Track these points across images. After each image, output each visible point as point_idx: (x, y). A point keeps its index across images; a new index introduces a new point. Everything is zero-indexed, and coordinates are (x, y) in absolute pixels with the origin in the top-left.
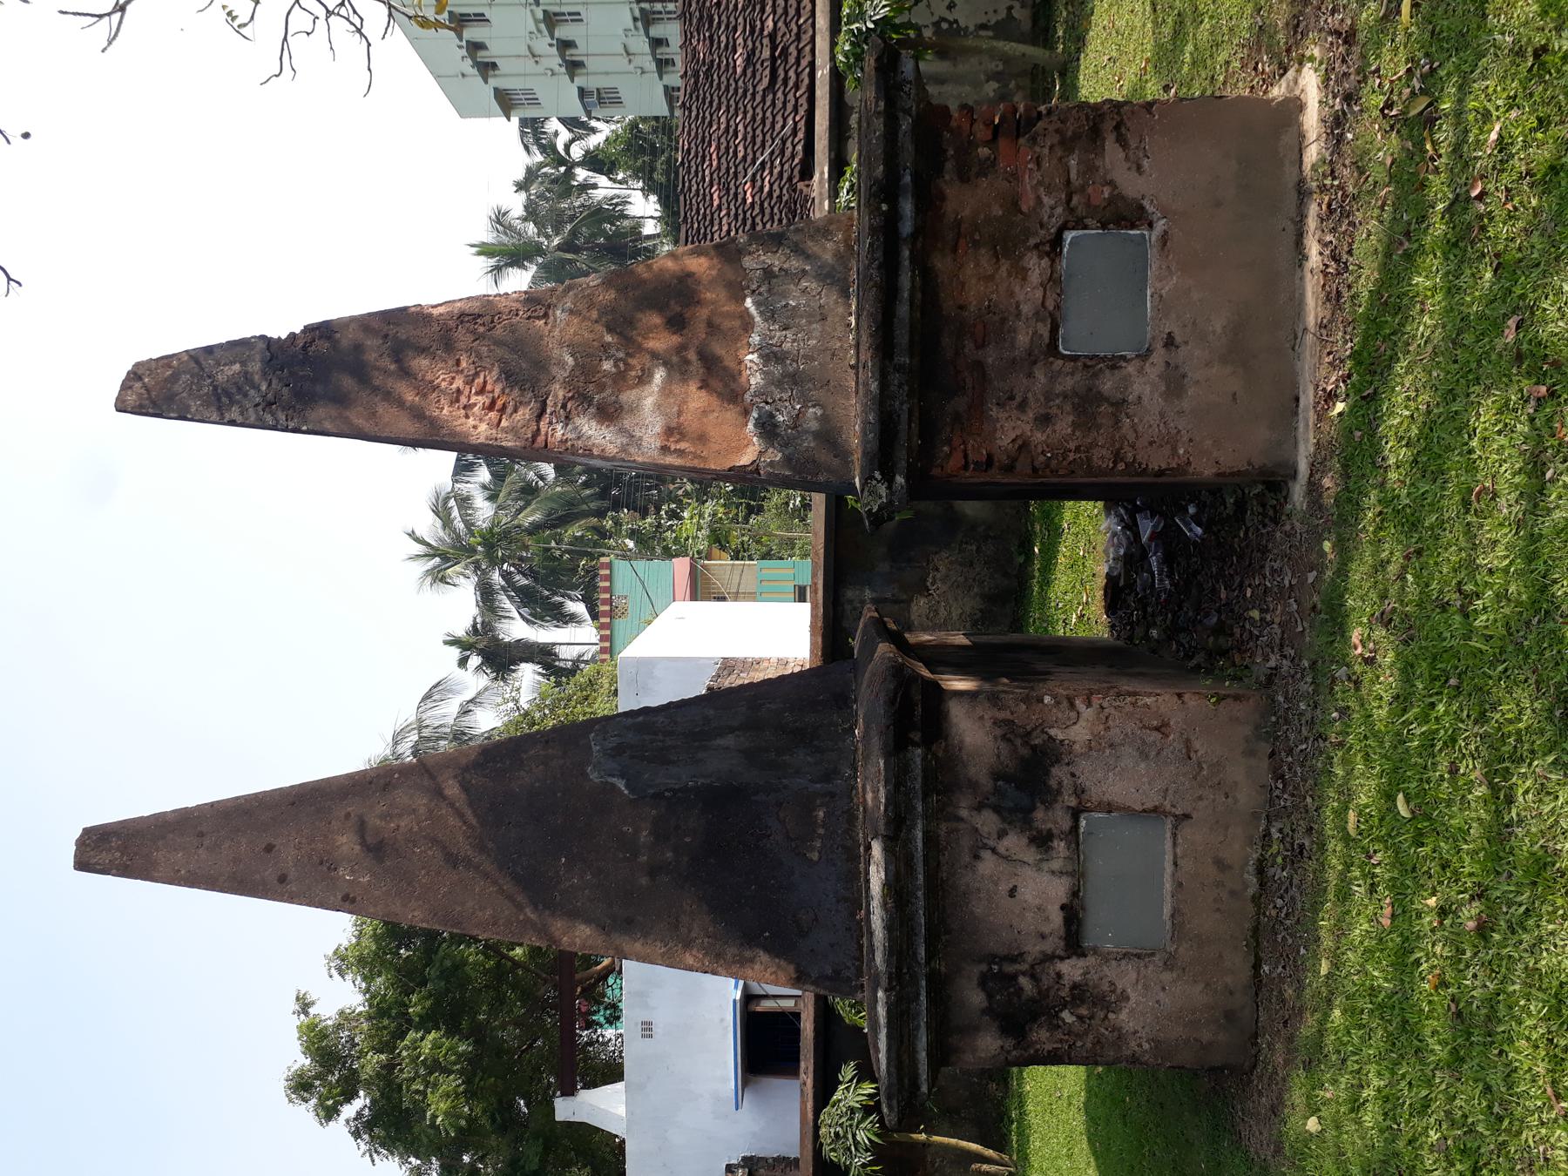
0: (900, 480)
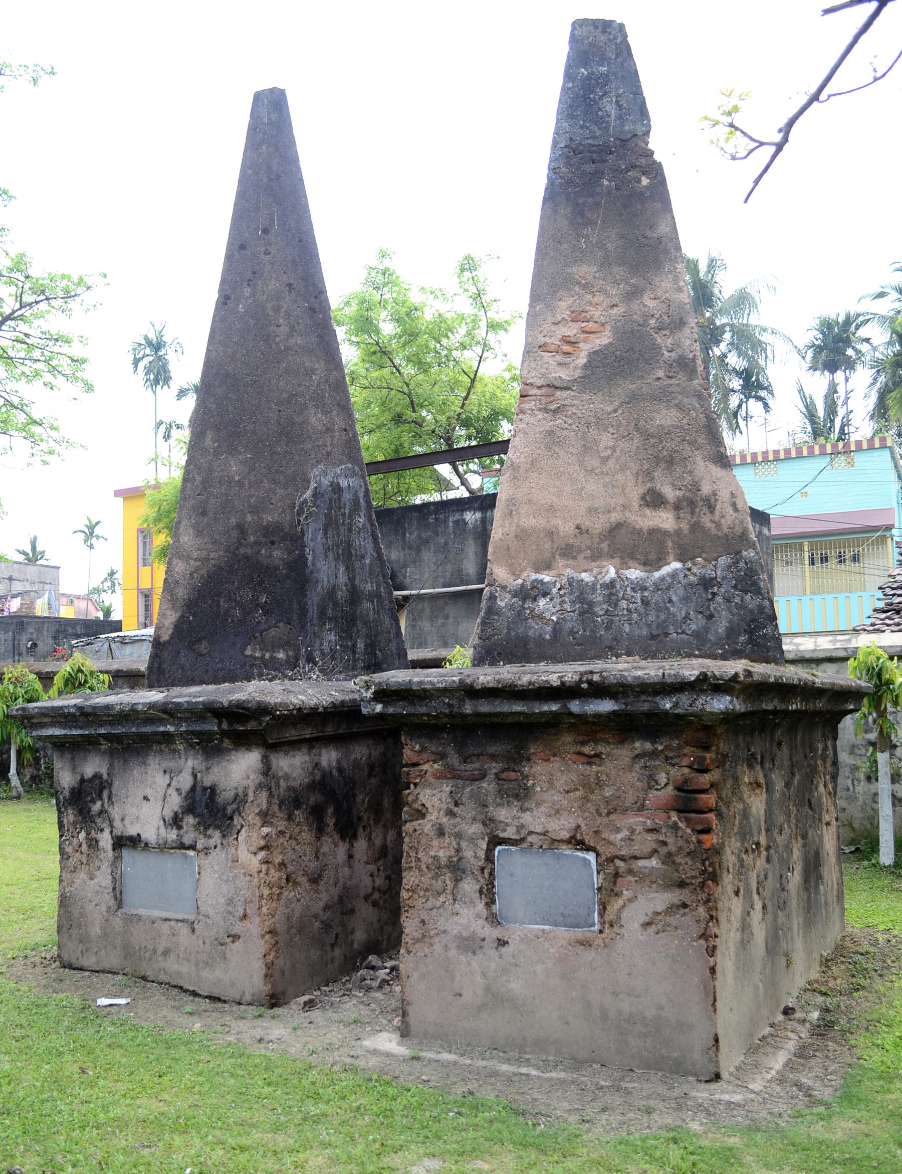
0: (379, 708)
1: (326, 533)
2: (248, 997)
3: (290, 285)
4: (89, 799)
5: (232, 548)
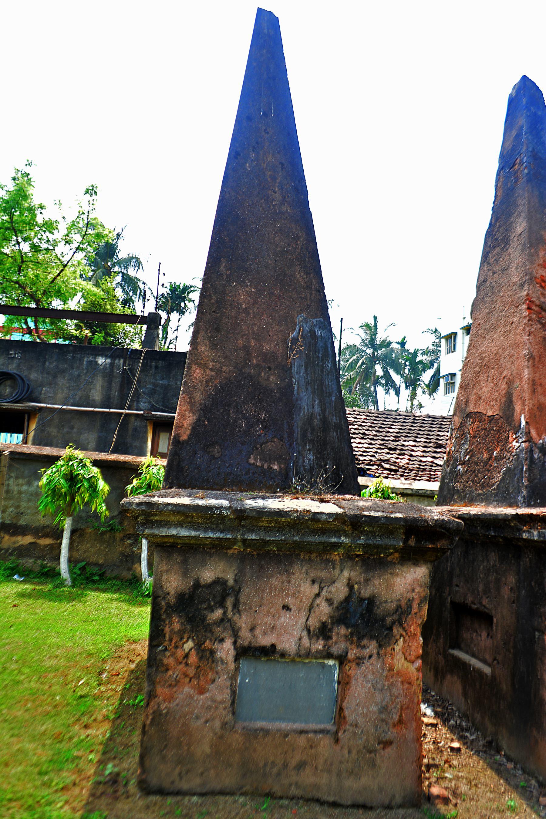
1: (306, 370)
2: (398, 799)
5: (240, 366)
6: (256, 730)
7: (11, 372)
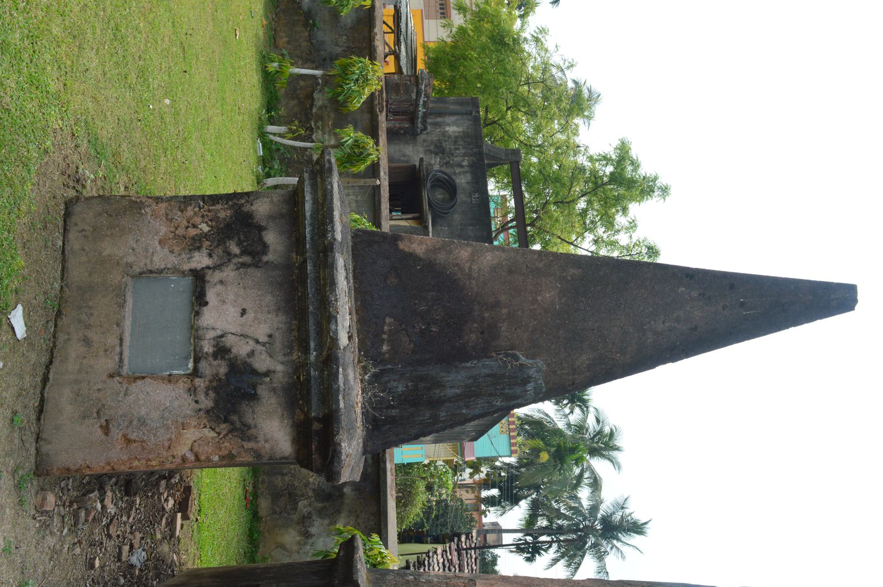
1: (488, 375)
2: (45, 448)
3: (696, 328)
4: (242, 237)
6: (125, 296)
7: (458, 196)
